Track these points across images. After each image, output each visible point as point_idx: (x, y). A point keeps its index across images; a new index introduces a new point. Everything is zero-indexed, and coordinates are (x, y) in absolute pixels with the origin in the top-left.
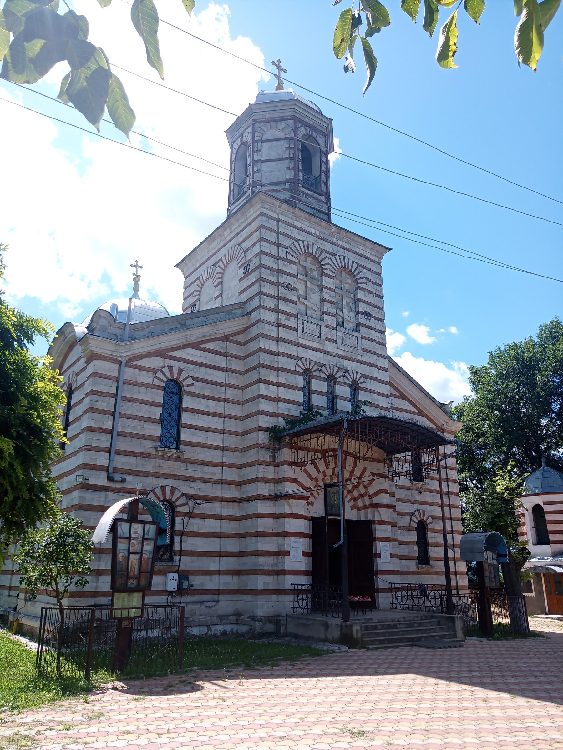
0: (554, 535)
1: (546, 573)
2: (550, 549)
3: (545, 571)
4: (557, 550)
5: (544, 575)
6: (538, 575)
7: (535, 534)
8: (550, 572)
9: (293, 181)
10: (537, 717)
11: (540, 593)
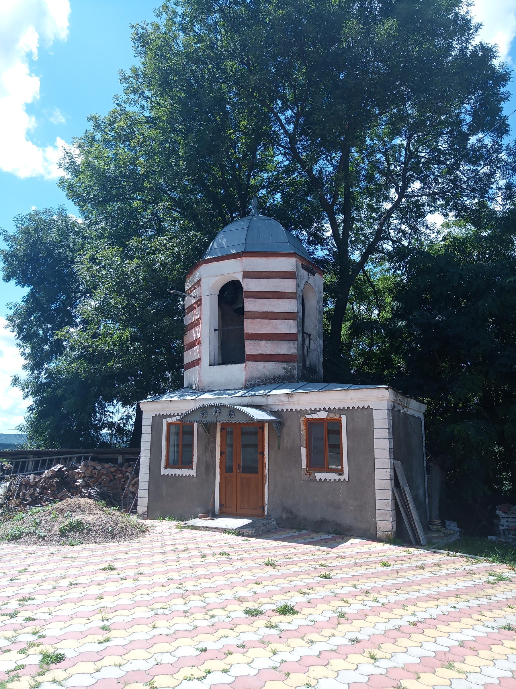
0: (256, 342)
1: (228, 424)
2: (244, 373)
3: (224, 418)
4: (257, 374)
5: (222, 429)
6: (208, 428)
7: (216, 343)
8: (238, 419)
9: (94, 137)
10: (225, 573)
11: (207, 468)
